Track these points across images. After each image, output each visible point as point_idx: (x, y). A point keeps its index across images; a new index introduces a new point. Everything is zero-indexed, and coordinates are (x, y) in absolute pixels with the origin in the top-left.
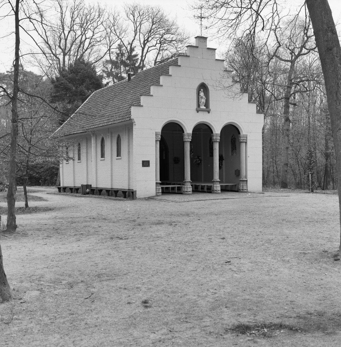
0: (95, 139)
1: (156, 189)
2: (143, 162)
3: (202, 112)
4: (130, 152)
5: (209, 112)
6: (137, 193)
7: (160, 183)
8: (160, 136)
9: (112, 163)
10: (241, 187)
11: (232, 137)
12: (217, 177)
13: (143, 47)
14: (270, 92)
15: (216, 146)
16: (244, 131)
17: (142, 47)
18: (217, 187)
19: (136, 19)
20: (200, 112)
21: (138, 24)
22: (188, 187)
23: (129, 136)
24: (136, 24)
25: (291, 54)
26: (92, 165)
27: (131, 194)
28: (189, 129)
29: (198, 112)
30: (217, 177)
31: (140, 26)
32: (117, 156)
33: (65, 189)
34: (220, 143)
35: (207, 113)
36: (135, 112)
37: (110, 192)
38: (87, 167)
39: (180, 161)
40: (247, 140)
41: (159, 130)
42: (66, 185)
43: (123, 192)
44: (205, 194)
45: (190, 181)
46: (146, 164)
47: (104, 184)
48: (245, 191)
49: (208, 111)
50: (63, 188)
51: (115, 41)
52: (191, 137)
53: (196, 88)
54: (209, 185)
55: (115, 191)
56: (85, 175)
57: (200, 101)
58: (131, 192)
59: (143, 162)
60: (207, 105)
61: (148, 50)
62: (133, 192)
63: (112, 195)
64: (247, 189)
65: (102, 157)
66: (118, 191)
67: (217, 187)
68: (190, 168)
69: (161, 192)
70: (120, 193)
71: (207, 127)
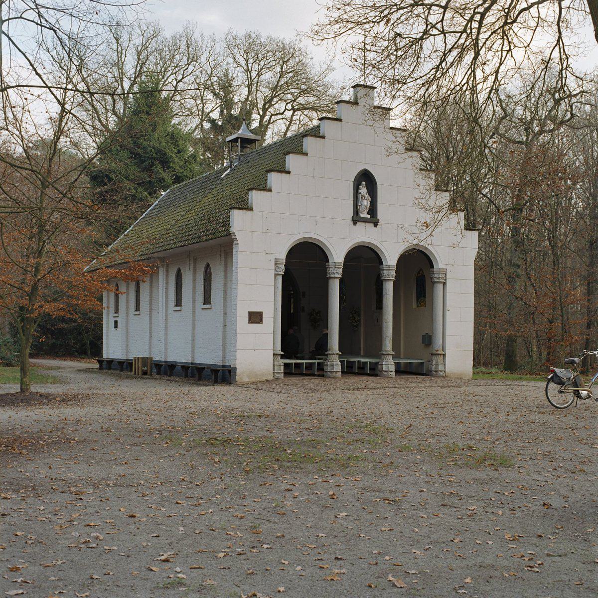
0: (165, 271)
1: (274, 365)
2: (260, 314)
3: (363, 224)
4: (228, 294)
5: (376, 226)
6: (238, 372)
7: (281, 355)
8: (283, 267)
9: (194, 316)
10: (433, 367)
11: (419, 273)
12: (388, 346)
13: (261, 113)
14: (487, 197)
15: (389, 288)
16: (441, 260)
17: (259, 114)
18: (389, 365)
19: (250, 66)
20: (358, 223)
21: (254, 74)
22: (335, 364)
23: (226, 266)
24: (250, 74)
25: (526, 130)
26: (159, 316)
27: (227, 373)
28: (337, 255)
29: (355, 224)
30: (388, 346)
31: (258, 78)
32: (204, 304)
33: (110, 362)
34: (395, 283)
35: (372, 225)
36: (238, 219)
37: (189, 371)
38: (151, 323)
39: (320, 318)
40: (445, 280)
41: (283, 256)
42: (112, 356)
43: (183, 367)
44: (365, 378)
45: (338, 352)
46: (255, 318)
47: (179, 355)
48: (441, 373)
49: (374, 223)
50: (107, 361)
51: (214, 108)
52: (341, 270)
53: (353, 180)
54: (374, 360)
55: (197, 368)
56: (148, 337)
57: (359, 204)
58: (227, 371)
59: (260, 314)
60: (373, 211)
61: (270, 120)
62: (230, 371)
63: (193, 376)
64: (445, 371)
65: (176, 306)
66: (203, 369)
67: (389, 365)
68: (338, 340)
69: (282, 371)
70: (207, 372)
71: (374, 255)
